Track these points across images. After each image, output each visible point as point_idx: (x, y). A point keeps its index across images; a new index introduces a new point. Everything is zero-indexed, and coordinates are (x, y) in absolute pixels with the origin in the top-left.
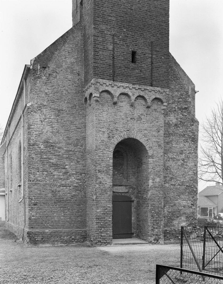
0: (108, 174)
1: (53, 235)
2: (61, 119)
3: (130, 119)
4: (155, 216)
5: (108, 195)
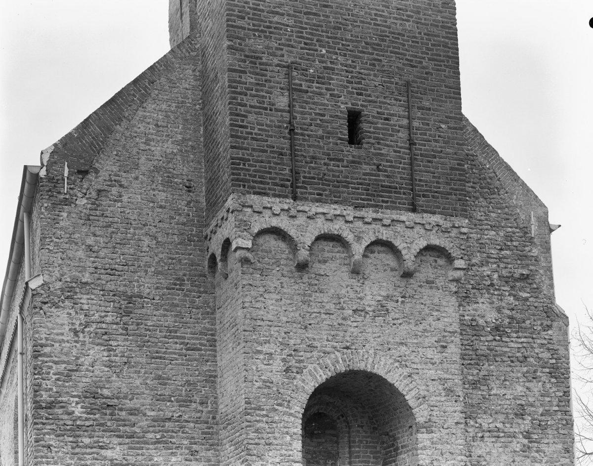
3: (350, 312)
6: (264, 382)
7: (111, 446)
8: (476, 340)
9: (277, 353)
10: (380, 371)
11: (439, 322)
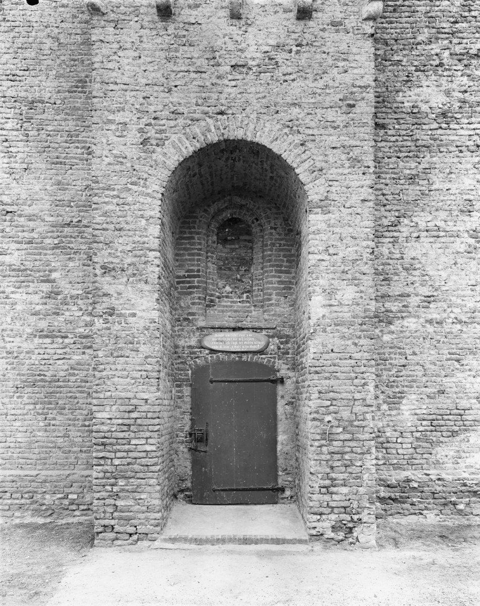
0: (140, 280)
1: (7, 489)
2: (38, 130)
3: (228, 68)
4: (337, 437)
5: (141, 356)
6: (115, 157)
7: (9, 252)
8: (417, 129)
9: (132, 122)
10: (264, 140)
11: (346, 74)
